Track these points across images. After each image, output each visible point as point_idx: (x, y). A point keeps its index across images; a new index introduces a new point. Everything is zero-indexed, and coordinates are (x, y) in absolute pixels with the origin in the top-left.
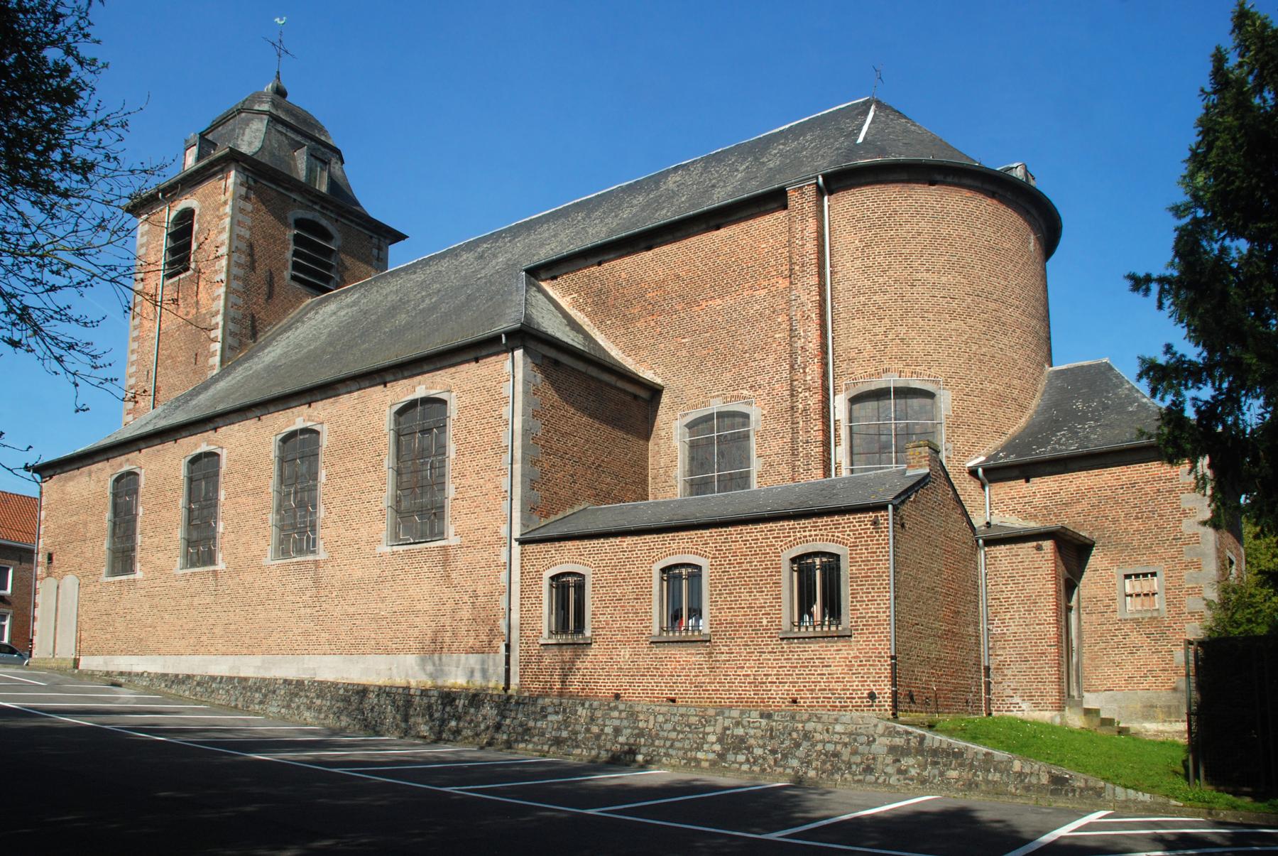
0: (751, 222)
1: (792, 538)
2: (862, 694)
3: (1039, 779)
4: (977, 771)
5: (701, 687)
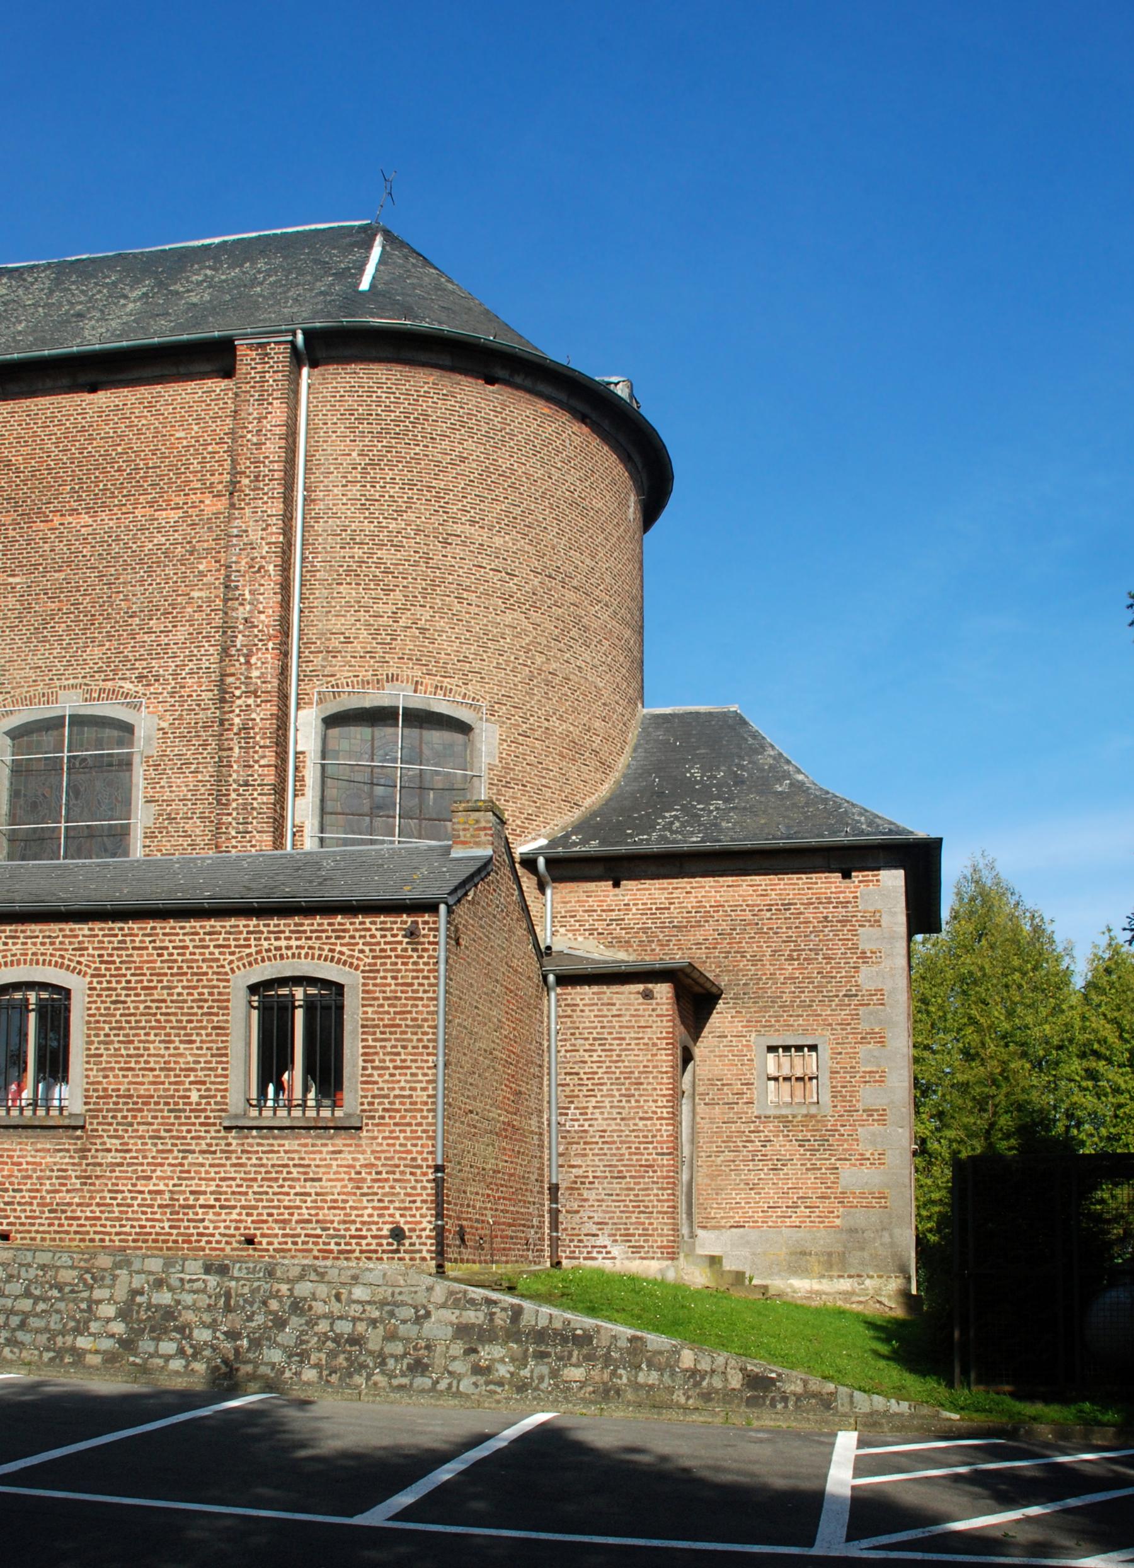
0: (159, 388)
1: (253, 950)
2: (380, 1229)
3: (726, 1380)
5: (64, 1212)
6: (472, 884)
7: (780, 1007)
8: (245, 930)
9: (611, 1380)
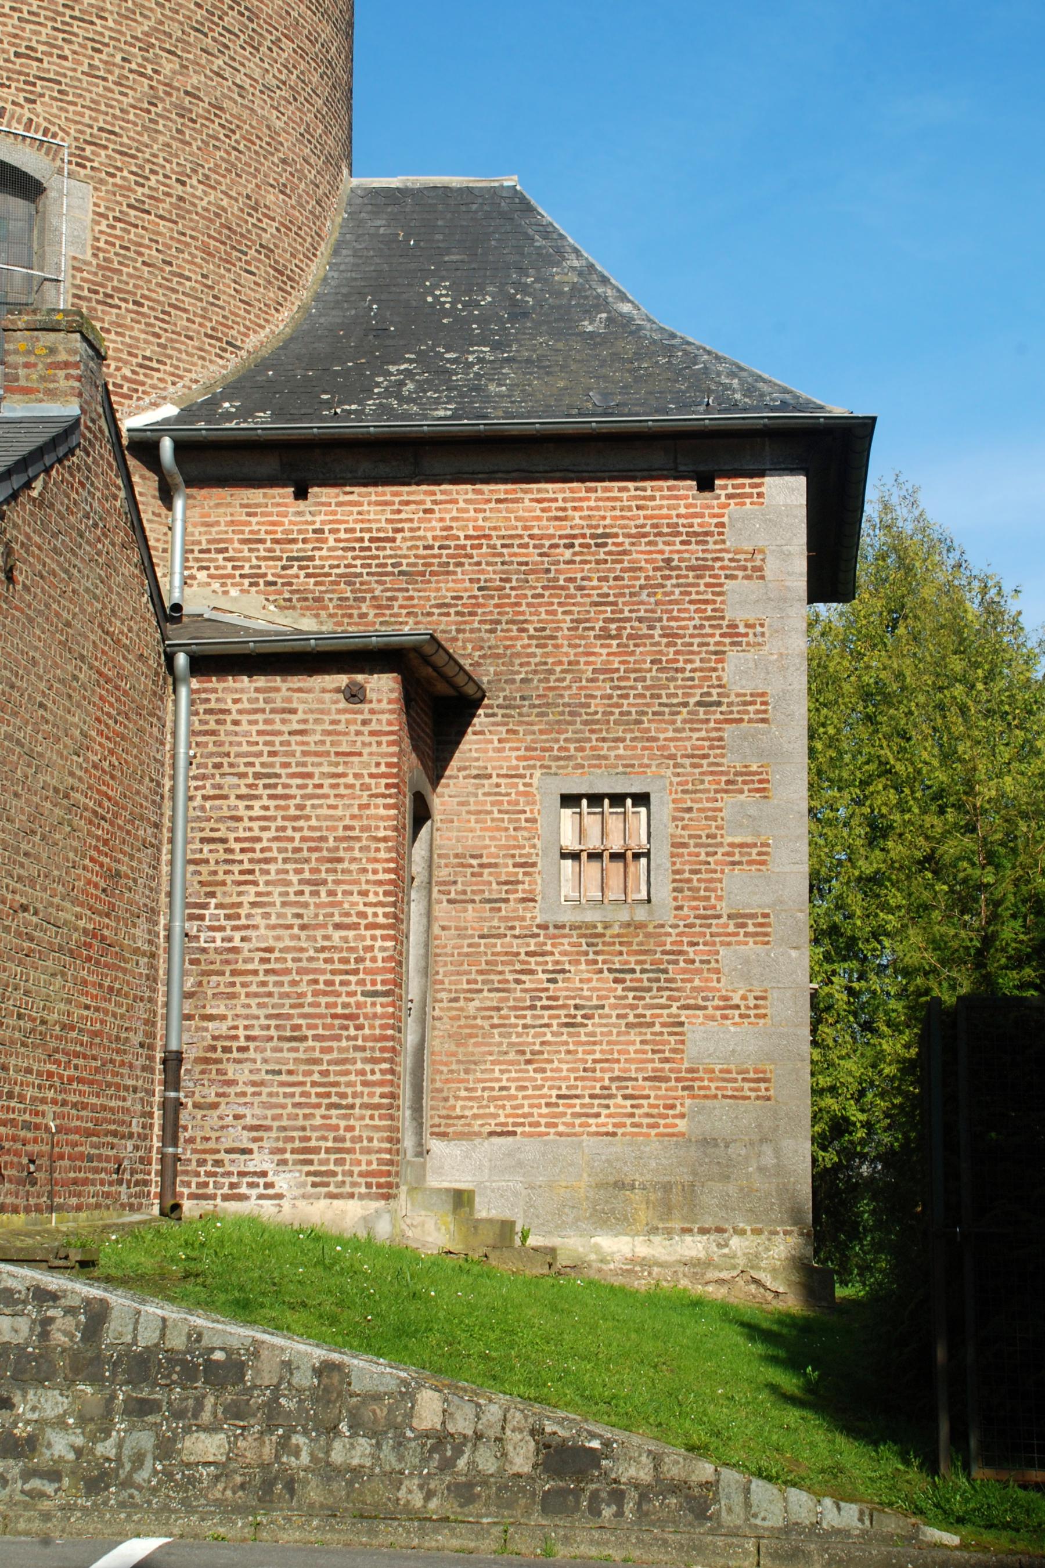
3: (504, 1455)
4: (291, 1431)
6: (40, 467)
7: (586, 723)
9: (278, 1457)
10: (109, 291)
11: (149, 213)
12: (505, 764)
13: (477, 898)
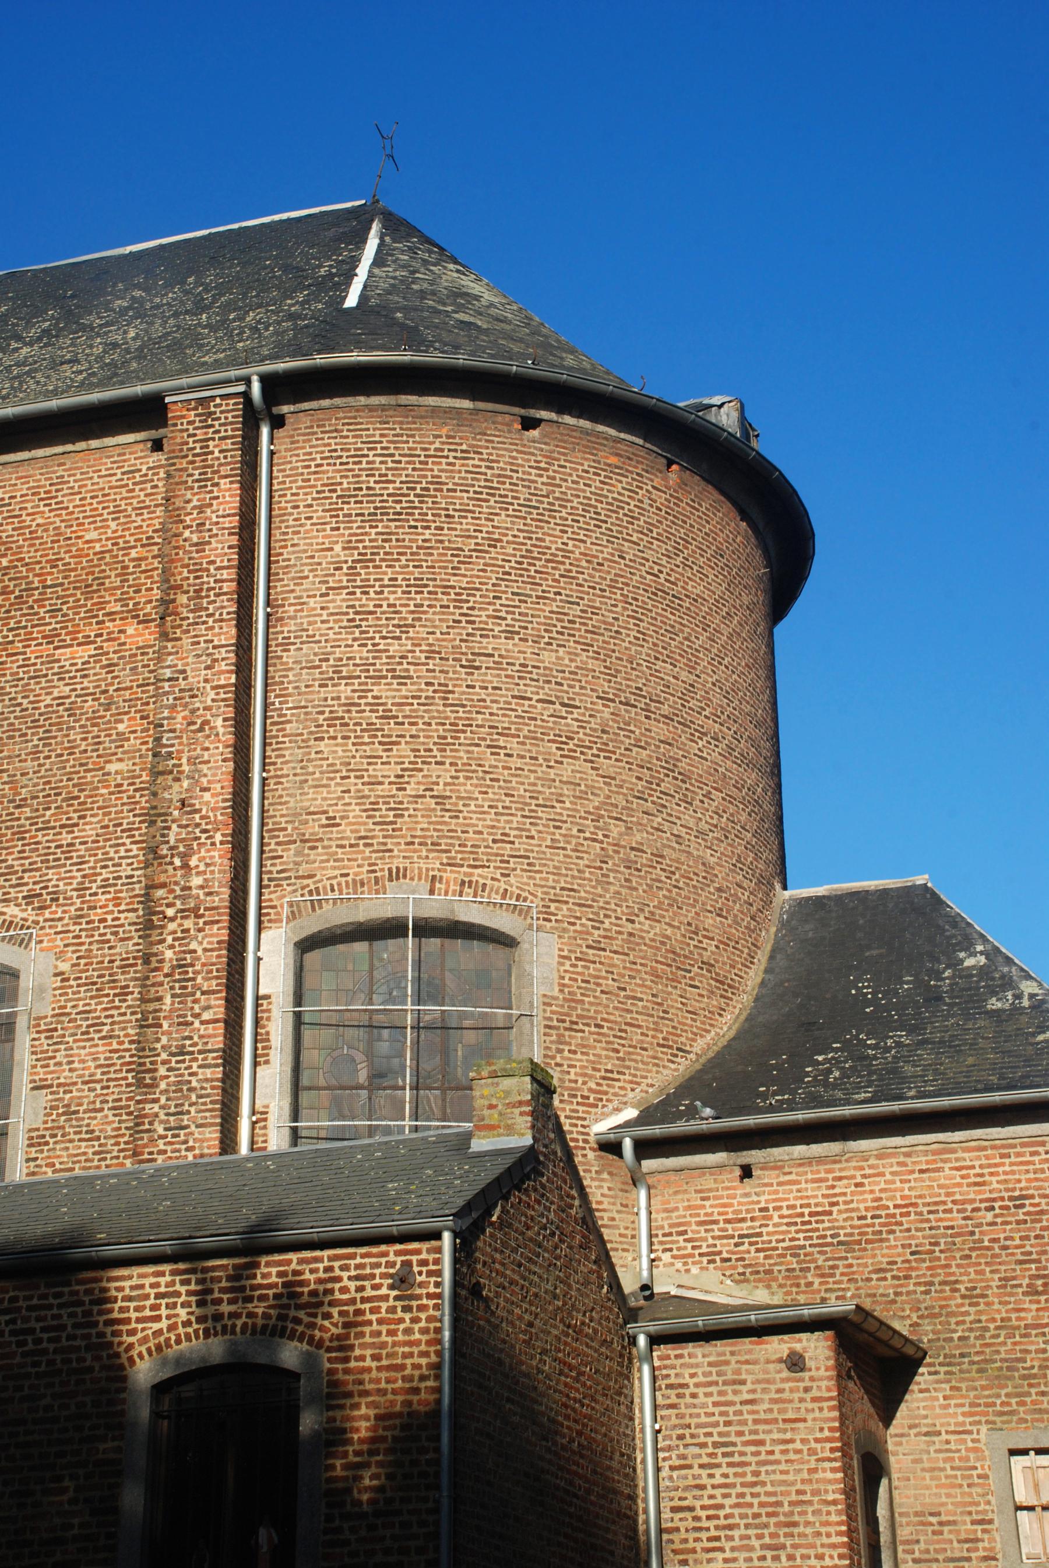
1: (164, 1324)
7: (1024, 1377)
8: (153, 1292)
10: (574, 1019)
11: (604, 950)
12: (952, 1421)
13: (941, 1557)
